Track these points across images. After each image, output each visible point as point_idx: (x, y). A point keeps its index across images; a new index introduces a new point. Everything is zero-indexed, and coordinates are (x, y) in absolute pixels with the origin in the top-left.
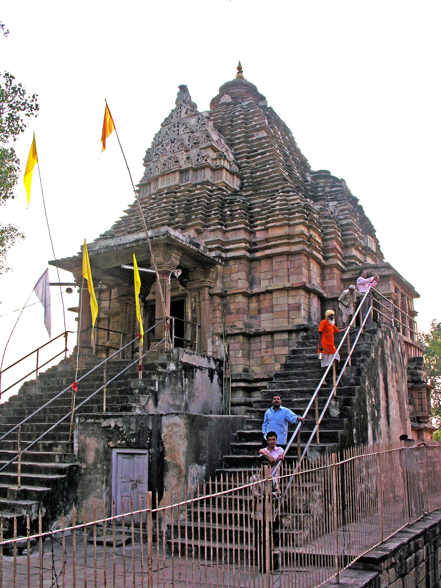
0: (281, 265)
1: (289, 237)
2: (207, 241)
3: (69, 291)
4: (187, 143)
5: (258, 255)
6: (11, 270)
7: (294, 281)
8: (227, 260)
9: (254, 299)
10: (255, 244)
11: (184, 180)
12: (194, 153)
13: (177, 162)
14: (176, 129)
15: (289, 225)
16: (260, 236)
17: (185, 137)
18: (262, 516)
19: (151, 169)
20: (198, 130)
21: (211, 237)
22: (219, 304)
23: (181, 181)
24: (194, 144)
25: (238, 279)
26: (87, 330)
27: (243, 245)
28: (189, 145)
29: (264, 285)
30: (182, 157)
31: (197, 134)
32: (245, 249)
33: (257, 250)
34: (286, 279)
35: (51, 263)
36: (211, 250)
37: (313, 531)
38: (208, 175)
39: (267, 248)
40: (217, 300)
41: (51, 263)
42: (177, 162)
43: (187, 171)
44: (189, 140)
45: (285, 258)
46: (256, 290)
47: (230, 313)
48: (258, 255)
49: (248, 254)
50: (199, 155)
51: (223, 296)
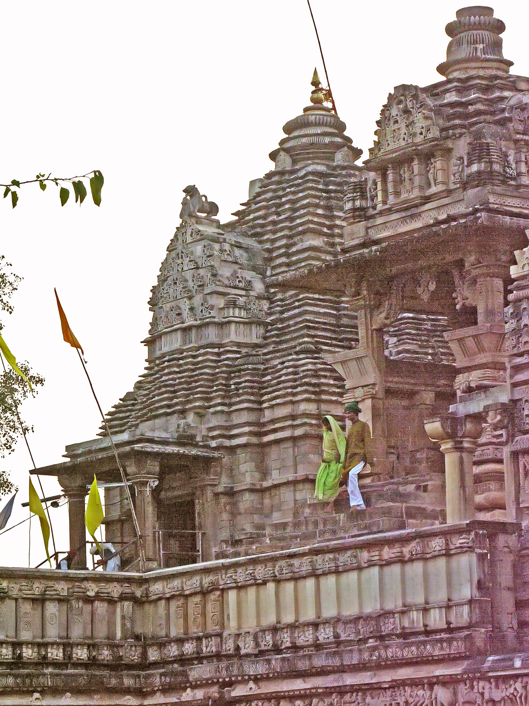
0: (288, 451)
1: (293, 417)
3: (55, 505)
4: (190, 284)
5: (266, 439)
6: (30, 431)
8: (232, 450)
9: (267, 494)
10: (264, 425)
11: (188, 342)
13: (179, 314)
14: (179, 261)
15: (292, 403)
16: (268, 415)
20: (204, 266)
21: (214, 422)
22: (225, 504)
23: (184, 343)
24: (199, 286)
25: (247, 472)
26: (79, 549)
27: (247, 429)
28: (193, 287)
29: (276, 477)
31: (201, 272)
32: (250, 433)
33: (266, 433)
34: (292, 470)
35: (32, 472)
36: (213, 438)
38: (212, 335)
39: (275, 431)
40: (223, 500)
41: (32, 472)
42: (179, 314)
43: (189, 328)
44: (193, 281)
45: (289, 444)
46: (266, 484)
47: (240, 514)
48: (266, 439)
49: (254, 440)
50: (202, 305)
51: (231, 493)
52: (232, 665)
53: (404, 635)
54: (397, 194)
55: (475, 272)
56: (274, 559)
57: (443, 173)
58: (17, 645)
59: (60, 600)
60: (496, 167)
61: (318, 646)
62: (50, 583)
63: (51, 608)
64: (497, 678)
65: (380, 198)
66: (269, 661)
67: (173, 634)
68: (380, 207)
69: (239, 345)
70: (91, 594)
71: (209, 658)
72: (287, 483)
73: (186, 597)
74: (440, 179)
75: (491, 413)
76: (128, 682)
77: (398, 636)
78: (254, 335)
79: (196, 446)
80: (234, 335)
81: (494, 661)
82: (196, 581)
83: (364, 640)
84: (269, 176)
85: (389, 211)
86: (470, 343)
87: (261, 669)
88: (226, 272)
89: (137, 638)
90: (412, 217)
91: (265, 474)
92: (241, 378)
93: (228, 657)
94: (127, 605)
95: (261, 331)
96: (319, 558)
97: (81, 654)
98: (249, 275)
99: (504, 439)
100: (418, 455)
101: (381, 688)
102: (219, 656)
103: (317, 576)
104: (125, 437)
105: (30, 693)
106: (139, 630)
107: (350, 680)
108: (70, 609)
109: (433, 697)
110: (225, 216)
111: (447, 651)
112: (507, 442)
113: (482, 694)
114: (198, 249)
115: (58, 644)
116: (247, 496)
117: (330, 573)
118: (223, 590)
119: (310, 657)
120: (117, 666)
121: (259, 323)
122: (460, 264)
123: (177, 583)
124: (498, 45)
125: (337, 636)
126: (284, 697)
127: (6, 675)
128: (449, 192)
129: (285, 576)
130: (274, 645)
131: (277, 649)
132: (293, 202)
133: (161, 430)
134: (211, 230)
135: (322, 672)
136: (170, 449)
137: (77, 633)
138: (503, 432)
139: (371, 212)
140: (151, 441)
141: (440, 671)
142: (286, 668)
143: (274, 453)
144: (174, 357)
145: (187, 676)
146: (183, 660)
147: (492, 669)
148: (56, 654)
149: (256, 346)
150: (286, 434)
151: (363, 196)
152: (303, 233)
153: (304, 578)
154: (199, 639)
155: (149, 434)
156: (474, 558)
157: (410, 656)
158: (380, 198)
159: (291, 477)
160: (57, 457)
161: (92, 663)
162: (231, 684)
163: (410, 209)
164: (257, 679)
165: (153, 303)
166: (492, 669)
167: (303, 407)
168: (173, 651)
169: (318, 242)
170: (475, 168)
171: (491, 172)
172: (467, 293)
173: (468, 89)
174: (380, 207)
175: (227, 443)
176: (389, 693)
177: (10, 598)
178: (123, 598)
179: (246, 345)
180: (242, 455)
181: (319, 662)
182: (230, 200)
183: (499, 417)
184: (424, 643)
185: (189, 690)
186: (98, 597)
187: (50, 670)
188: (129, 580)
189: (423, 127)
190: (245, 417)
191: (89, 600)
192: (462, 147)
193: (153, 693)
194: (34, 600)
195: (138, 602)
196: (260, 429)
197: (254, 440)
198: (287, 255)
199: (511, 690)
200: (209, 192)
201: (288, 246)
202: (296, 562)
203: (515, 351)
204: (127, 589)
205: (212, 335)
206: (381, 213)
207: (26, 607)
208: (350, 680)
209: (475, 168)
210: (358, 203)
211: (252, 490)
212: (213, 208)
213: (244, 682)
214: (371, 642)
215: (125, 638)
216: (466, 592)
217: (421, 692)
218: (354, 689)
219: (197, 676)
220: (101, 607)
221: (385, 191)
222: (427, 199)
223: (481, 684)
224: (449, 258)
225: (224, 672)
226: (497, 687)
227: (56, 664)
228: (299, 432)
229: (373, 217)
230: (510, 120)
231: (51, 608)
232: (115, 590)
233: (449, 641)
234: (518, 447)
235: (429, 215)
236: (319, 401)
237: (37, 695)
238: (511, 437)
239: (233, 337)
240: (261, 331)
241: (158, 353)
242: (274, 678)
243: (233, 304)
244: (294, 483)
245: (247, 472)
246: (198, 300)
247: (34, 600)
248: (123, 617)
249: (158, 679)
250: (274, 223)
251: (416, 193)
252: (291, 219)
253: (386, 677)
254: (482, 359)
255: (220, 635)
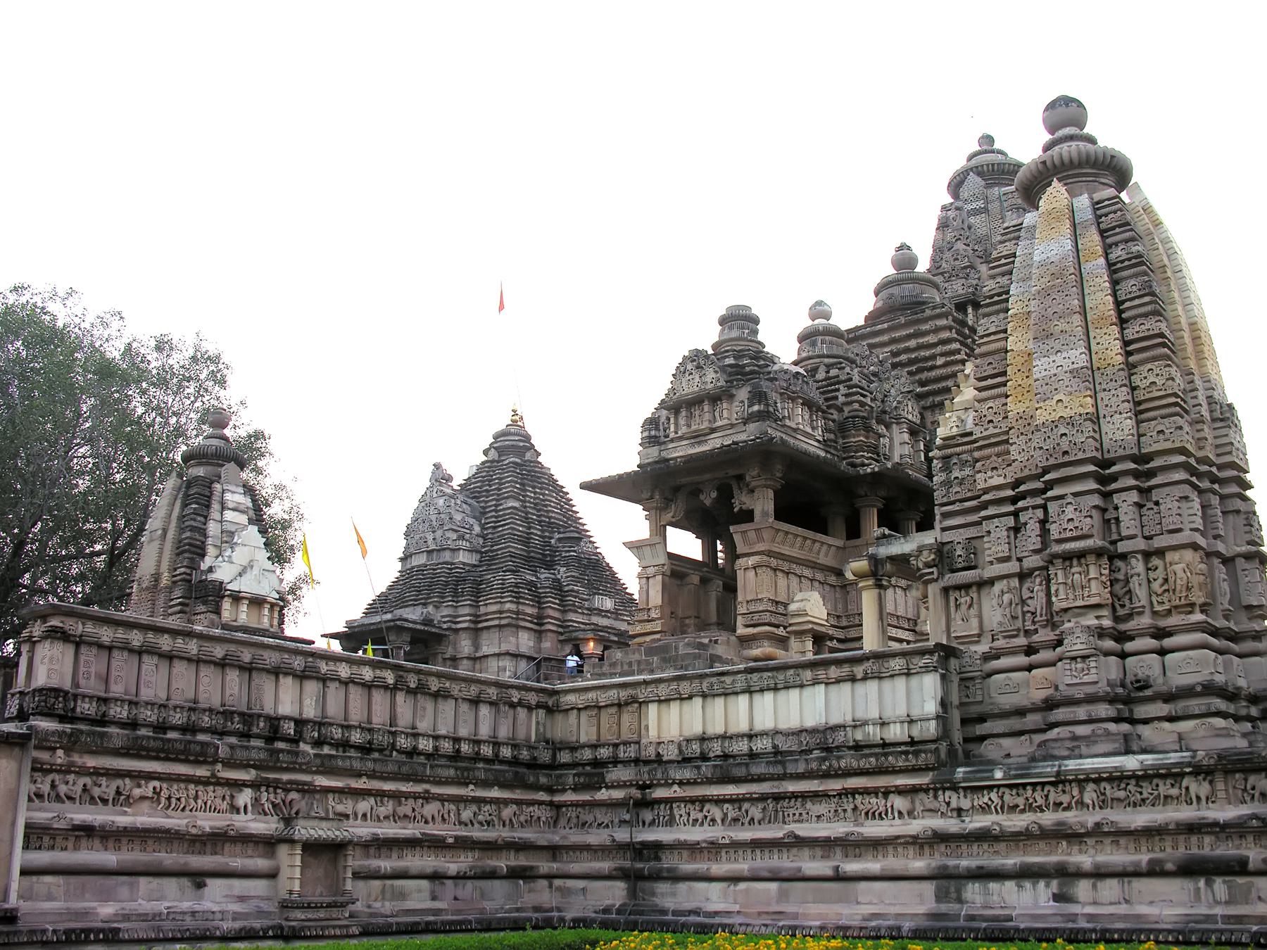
0: (495, 635)
1: (501, 612)
2: (440, 614)
5: (480, 625)
7: (504, 648)
8: (457, 631)
12: (439, 533)
16: (483, 610)
17: (433, 518)
18: (399, 710)
19: (426, 822)
30: (430, 537)
37: (984, 506)
39: (487, 620)
43: (432, 551)
46: (478, 655)
48: (480, 625)
49: (472, 626)
52: (655, 769)
53: (857, 747)
54: (689, 426)
55: (753, 484)
56: (702, 677)
57: (730, 412)
58: (457, 740)
59: (491, 703)
60: (771, 409)
61: (752, 755)
62: (483, 687)
63: (484, 710)
64: (965, 789)
65: (672, 429)
66: (698, 768)
67: (583, 739)
68: (672, 435)
69: (464, 564)
70: (515, 700)
71: (626, 763)
72: (494, 655)
73: (600, 708)
74: (725, 415)
75: (925, 553)
76: (543, 780)
77: (849, 748)
78: (472, 559)
79: (434, 626)
80: (463, 557)
81: (965, 773)
82: (613, 693)
83: (811, 751)
84: (483, 463)
85: (681, 438)
86: (752, 535)
87: (687, 774)
88: (458, 517)
89: (547, 742)
90: (699, 443)
91: (477, 647)
92: (463, 585)
93: (647, 762)
94: (542, 712)
95: (479, 556)
96: (755, 676)
97: (506, 752)
98: (472, 521)
99: (935, 576)
100: (687, 621)
101: (829, 796)
102: (637, 761)
103: (751, 693)
104: (389, 616)
105: (467, 785)
106: (549, 736)
107: (792, 787)
108: (498, 711)
109: (889, 805)
110: (455, 484)
111: (914, 762)
112: (936, 580)
113: (948, 804)
114: (441, 502)
115: (507, 744)
116: (465, 662)
117: (743, 692)
118: (640, 703)
119: (747, 765)
120: (533, 765)
121: (477, 552)
122: (740, 478)
123: (592, 695)
124: (756, 332)
125: (775, 746)
126: (709, 801)
127: (449, 767)
128: (732, 426)
129: (715, 692)
130: (701, 753)
131: (704, 757)
132: (500, 479)
133: (413, 614)
134: (449, 491)
135: (760, 779)
136: (418, 627)
137: (503, 733)
138: (934, 569)
139: (663, 439)
140: (406, 620)
141: (901, 781)
142: (718, 773)
143: (485, 635)
144: (421, 569)
145: (604, 778)
146: (596, 763)
147: (965, 780)
148: (487, 751)
149: (474, 566)
150: (496, 622)
151: (657, 429)
152: (507, 498)
153: (736, 693)
154: (616, 746)
155: (405, 616)
156: (938, 677)
157: (867, 766)
158: (672, 429)
159: (497, 651)
160: (340, 628)
161: (515, 762)
162: (649, 787)
163: (698, 437)
164: (681, 783)
165: (407, 535)
166: (965, 780)
167: (508, 606)
168: (587, 754)
169: (516, 504)
170: (756, 408)
171: (768, 412)
172: (744, 499)
173: (744, 356)
174: (672, 435)
175: (454, 626)
176: (835, 800)
177: (452, 697)
178: (538, 706)
179: (468, 565)
180: (463, 635)
181: (757, 769)
182: (460, 474)
183: (933, 556)
184: (886, 755)
185: (604, 790)
186: (520, 703)
187: (481, 765)
188: (543, 690)
189: (711, 379)
190: (467, 610)
191: (513, 706)
192: (743, 394)
193: (564, 791)
194: (470, 701)
195: (550, 711)
196: (476, 619)
197: (472, 626)
198: (496, 511)
199: (986, 800)
200: (449, 468)
201: (496, 506)
202: (728, 679)
203: (945, 500)
204: (543, 698)
205: (447, 556)
206: (672, 441)
207: (464, 707)
208: (792, 787)
209: (756, 408)
210: (653, 433)
211: (468, 658)
212: (450, 479)
213: (668, 785)
214: (816, 753)
215: (538, 741)
216: (931, 707)
217: (874, 800)
218: (794, 796)
219: (614, 778)
220: (522, 712)
221: (676, 424)
222: (713, 430)
223: (948, 793)
224: (732, 472)
225: (646, 776)
226: (965, 797)
227: (487, 761)
228: (504, 622)
229: (664, 443)
230: (776, 379)
231: (484, 710)
232: (532, 698)
233: (916, 754)
234: (946, 584)
235: (714, 442)
236: (518, 603)
237: (471, 787)
238: (941, 574)
239: (461, 558)
240: (479, 556)
241: (409, 566)
242: (702, 783)
243: (462, 538)
244: (498, 655)
245: (465, 646)
246: (439, 533)
247: (470, 701)
248: (538, 723)
249: (571, 778)
250: (487, 491)
251: (705, 425)
252: (499, 489)
253: (835, 785)
254: (761, 547)
255: (638, 743)
